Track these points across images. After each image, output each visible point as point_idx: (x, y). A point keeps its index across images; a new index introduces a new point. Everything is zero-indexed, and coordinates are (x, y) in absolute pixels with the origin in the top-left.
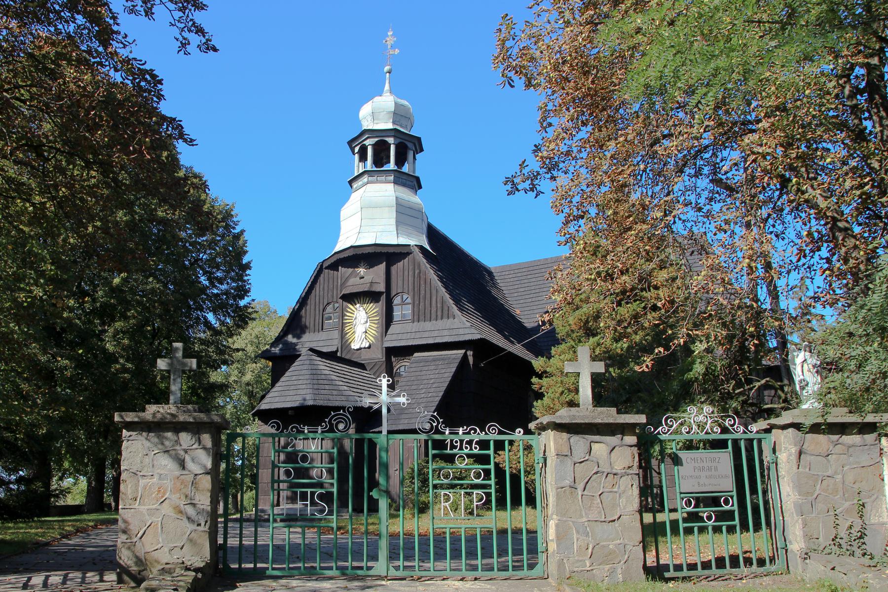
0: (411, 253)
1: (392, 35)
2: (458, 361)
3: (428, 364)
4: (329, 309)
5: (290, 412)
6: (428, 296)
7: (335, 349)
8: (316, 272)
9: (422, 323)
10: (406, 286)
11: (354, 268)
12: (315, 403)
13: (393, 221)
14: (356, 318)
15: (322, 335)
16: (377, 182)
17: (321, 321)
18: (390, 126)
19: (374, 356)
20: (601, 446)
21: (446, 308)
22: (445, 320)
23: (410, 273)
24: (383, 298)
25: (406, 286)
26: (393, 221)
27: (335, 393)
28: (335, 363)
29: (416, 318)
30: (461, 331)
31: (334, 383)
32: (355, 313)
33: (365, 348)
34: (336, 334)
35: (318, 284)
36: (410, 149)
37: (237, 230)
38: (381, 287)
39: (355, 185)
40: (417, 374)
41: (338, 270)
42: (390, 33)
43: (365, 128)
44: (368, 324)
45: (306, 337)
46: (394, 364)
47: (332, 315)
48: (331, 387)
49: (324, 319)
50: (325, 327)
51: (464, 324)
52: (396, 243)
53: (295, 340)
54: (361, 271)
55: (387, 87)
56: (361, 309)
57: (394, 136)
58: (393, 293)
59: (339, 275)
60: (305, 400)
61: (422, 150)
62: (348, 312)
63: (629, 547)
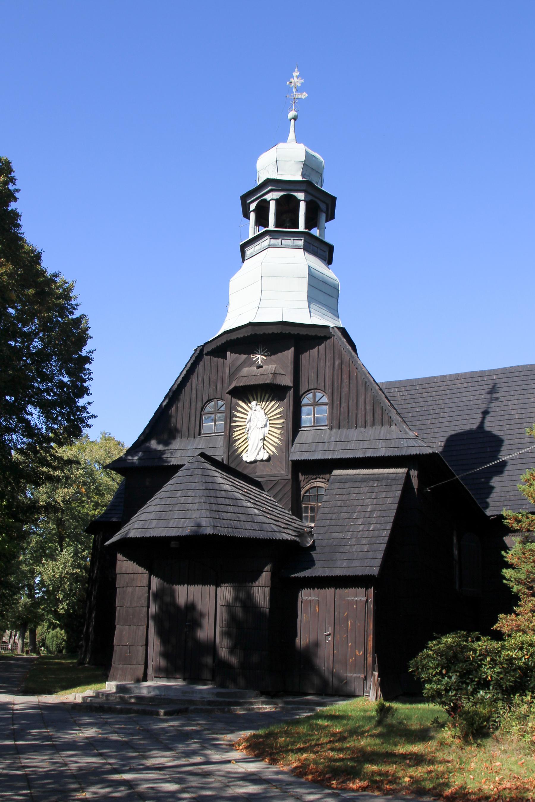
0: (330, 338)
1: (298, 77)
3: (357, 484)
4: (210, 407)
5: (173, 544)
8: (194, 358)
9: (344, 431)
11: (249, 354)
12: (216, 532)
16: (281, 246)
17: (198, 423)
18: (299, 178)
19: (274, 472)
21: (378, 412)
22: (377, 427)
23: (328, 364)
24: (290, 394)
27: (242, 517)
28: (232, 477)
31: (239, 503)
33: (262, 461)
35: (195, 374)
36: (322, 211)
37: (77, 314)
38: (287, 381)
39: (249, 251)
40: (344, 497)
41: (225, 358)
44: (268, 428)
45: (176, 444)
46: (302, 484)
48: (237, 509)
51: (406, 433)
53: (160, 447)
54: (259, 358)
57: (305, 192)
60: (199, 526)
62: (238, 411)
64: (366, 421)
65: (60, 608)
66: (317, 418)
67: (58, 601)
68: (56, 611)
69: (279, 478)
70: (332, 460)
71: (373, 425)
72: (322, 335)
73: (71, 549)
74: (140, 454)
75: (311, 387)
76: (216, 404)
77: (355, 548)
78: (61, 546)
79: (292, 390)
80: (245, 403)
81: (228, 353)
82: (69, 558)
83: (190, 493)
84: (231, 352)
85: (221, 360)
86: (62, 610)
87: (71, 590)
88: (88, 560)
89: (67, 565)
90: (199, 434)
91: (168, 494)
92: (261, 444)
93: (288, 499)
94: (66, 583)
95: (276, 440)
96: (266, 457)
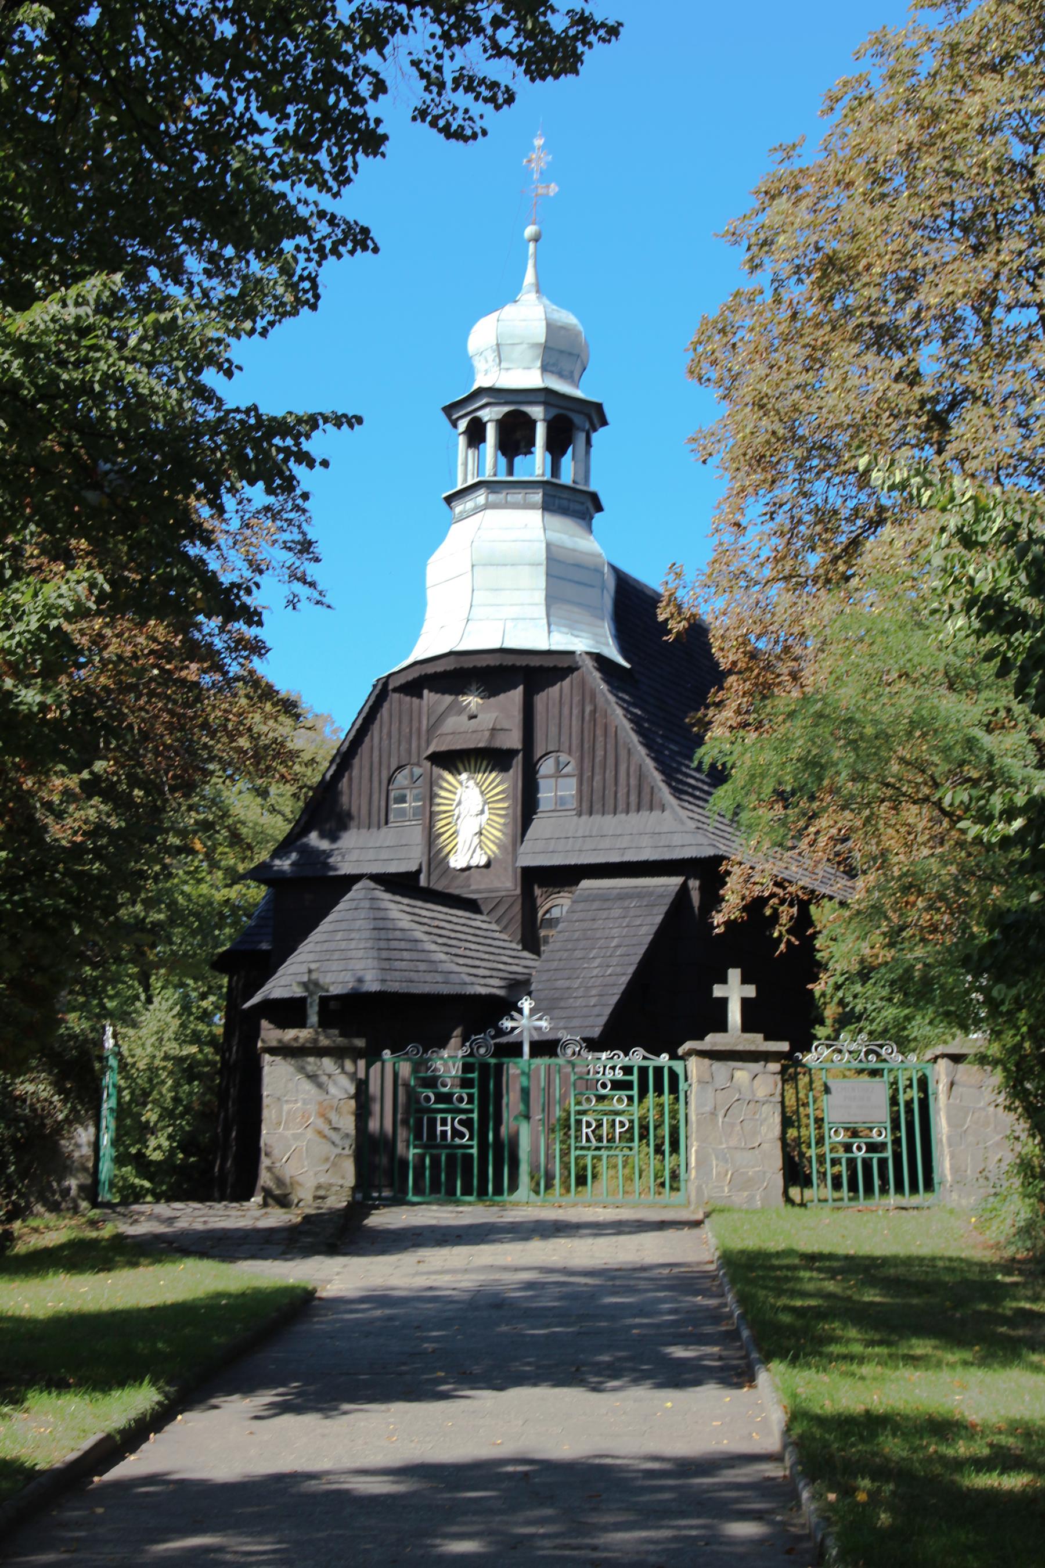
0: (577, 669)
1: (542, 148)
2: (669, 900)
3: (606, 905)
6: (611, 761)
7: (414, 868)
9: (597, 818)
10: (565, 738)
12: (384, 988)
13: (540, 597)
14: (459, 804)
15: (385, 836)
16: (506, 505)
17: (383, 804)
19: (497, 884)
20: (743, 1073)
21: (646, 790)
22: (644, 814)
23: (575, 711)
25: (565, 738)
26: (540, 596)
27: (422, 966)
28: (419, 903)
29: (585, 806)
30: (677, 840)
31: (420, 946)
32: (459, 792)
33: (477, 867)
34: (416, 835)
35: (377, 722)
38: (513, 740)
39: (459, 508)
40: (586, 925)
41: (420, 696)
42: (538, 142)
43: (482, 381)
44: (486, 815)
45: (350, 839)
46: (539, 901)
47: (408, 792)
48: (415, 955)
49: (391, 802)
50: (391, 818)
51: (682, 823)
52: (543, 646)
53: (324, 845)
54: (472, 701)
55: (530, 277)
56: (471, 783)
57: (546, 404)
58: (539, 752)
59: (425, 710)
60: (360, 980)
61: (604, 423)
62: (442, 788)
63: (768, 1175)
64: (628, 804)
65: (151, 1148)
66: (562, 798)
67: (145, 1130)
68: (140, 1155)
69: (503, 893)
70: (576, 867)
71: (638, 810)
72: (566, 665)
73: (173, 995)
74: (294, 856)
75: (550, 749)
76: (412, 774)
77: (579, 1002)
78: (147, 988)
79: (521, 755)
80: (450, 772)
81: (426, 692)
82: (169, 1019)
83: (353, 935)
84: (431, 691)
85: (415, 700)
86: (158, 1152)
87: (176, 1100)
88: (216, 1019)
89: (166, 1036)
90: (387, 823)
91: (324, 937)
92: (476, 840)
93: (516, 926)
94: (163, 1082)
95: (499, 834)
96: (483, 861)
